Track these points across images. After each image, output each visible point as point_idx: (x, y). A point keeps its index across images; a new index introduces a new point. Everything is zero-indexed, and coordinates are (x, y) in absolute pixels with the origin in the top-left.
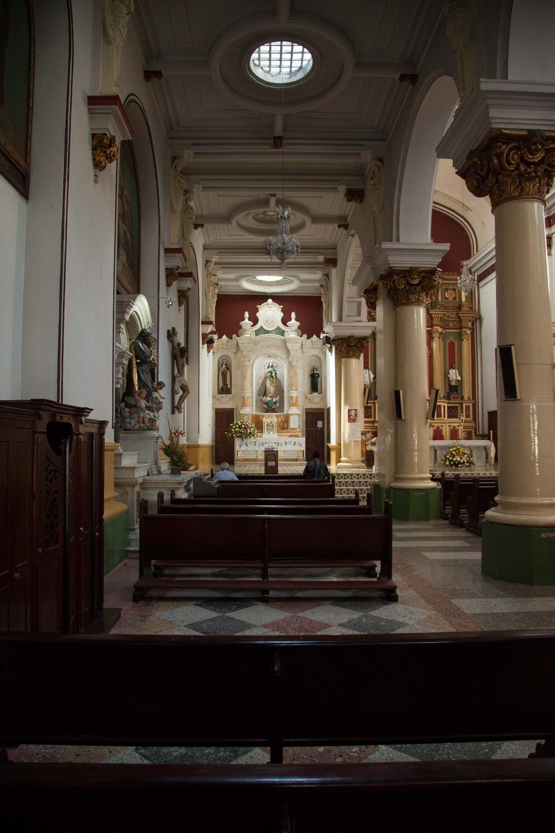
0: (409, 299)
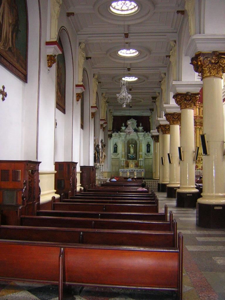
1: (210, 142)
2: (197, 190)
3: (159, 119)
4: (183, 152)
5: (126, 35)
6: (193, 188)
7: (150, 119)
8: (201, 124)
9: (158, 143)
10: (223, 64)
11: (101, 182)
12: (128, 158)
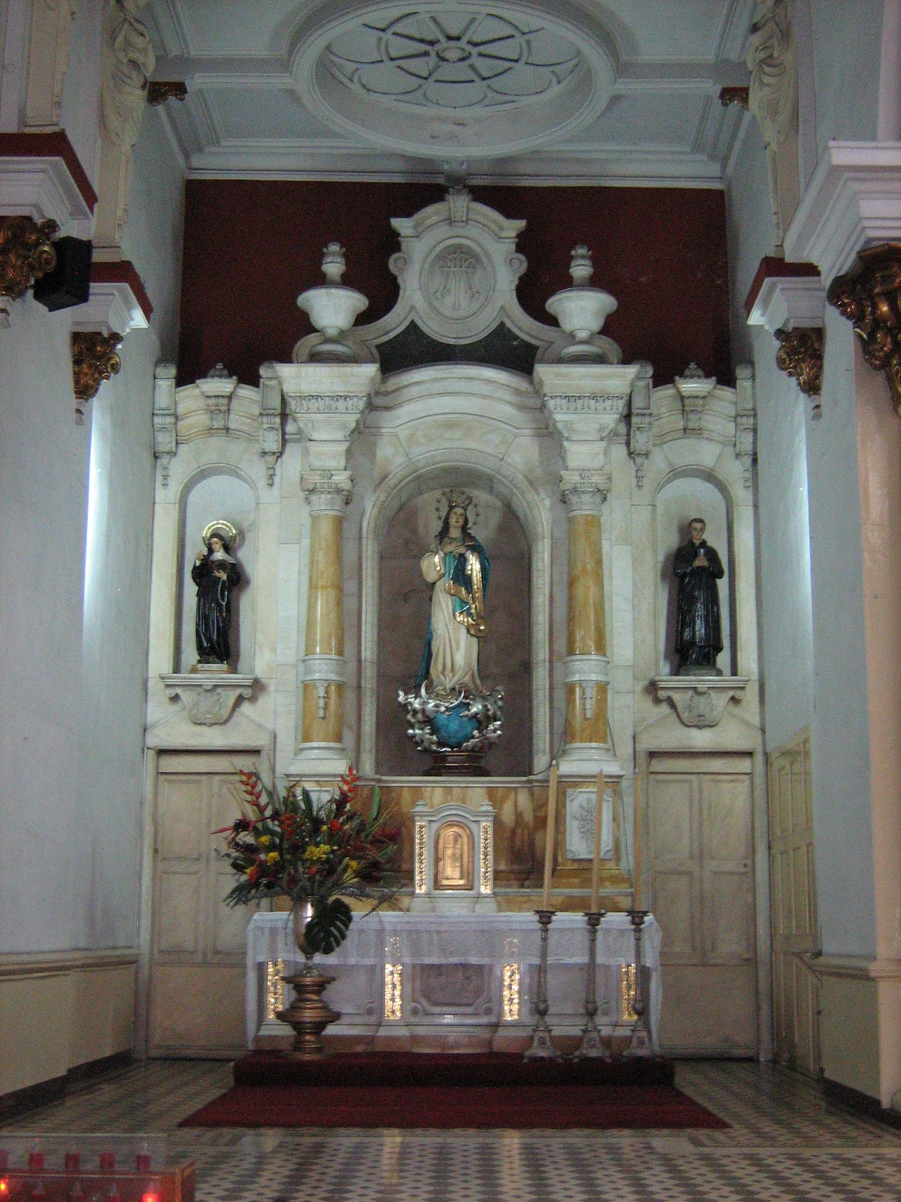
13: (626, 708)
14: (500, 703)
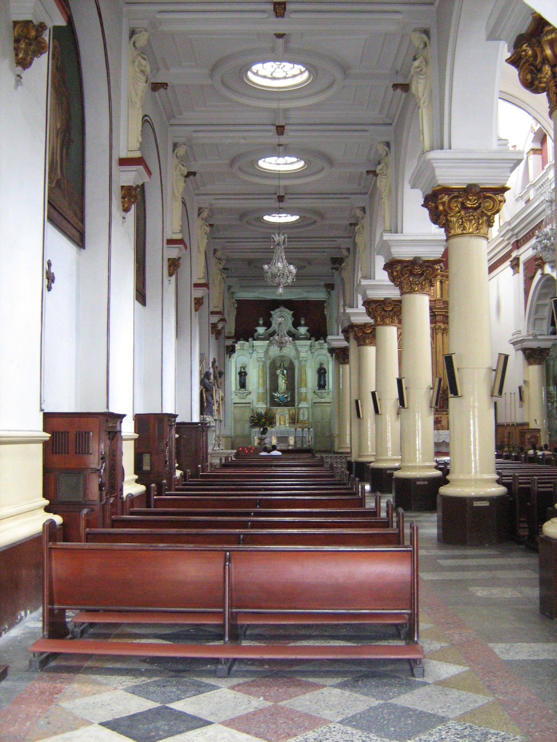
0: (384, 322)
1: (464, 370)
2: (438, 473)
3: (349, 310)
4: (406, 388)
5: (280, 130)
6: (429, 467)
7: (324, 307)
8: (446, 319)
9: (347, 367)
10: (488, 210)
11: (221, 460)
12: (274, 402)
13: (310, 396)
14: (303, 330)
